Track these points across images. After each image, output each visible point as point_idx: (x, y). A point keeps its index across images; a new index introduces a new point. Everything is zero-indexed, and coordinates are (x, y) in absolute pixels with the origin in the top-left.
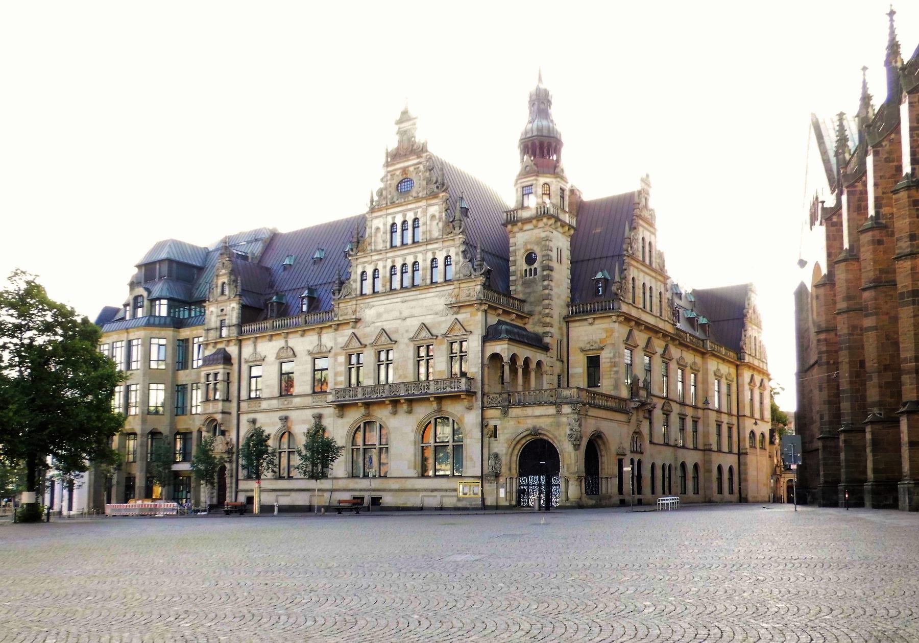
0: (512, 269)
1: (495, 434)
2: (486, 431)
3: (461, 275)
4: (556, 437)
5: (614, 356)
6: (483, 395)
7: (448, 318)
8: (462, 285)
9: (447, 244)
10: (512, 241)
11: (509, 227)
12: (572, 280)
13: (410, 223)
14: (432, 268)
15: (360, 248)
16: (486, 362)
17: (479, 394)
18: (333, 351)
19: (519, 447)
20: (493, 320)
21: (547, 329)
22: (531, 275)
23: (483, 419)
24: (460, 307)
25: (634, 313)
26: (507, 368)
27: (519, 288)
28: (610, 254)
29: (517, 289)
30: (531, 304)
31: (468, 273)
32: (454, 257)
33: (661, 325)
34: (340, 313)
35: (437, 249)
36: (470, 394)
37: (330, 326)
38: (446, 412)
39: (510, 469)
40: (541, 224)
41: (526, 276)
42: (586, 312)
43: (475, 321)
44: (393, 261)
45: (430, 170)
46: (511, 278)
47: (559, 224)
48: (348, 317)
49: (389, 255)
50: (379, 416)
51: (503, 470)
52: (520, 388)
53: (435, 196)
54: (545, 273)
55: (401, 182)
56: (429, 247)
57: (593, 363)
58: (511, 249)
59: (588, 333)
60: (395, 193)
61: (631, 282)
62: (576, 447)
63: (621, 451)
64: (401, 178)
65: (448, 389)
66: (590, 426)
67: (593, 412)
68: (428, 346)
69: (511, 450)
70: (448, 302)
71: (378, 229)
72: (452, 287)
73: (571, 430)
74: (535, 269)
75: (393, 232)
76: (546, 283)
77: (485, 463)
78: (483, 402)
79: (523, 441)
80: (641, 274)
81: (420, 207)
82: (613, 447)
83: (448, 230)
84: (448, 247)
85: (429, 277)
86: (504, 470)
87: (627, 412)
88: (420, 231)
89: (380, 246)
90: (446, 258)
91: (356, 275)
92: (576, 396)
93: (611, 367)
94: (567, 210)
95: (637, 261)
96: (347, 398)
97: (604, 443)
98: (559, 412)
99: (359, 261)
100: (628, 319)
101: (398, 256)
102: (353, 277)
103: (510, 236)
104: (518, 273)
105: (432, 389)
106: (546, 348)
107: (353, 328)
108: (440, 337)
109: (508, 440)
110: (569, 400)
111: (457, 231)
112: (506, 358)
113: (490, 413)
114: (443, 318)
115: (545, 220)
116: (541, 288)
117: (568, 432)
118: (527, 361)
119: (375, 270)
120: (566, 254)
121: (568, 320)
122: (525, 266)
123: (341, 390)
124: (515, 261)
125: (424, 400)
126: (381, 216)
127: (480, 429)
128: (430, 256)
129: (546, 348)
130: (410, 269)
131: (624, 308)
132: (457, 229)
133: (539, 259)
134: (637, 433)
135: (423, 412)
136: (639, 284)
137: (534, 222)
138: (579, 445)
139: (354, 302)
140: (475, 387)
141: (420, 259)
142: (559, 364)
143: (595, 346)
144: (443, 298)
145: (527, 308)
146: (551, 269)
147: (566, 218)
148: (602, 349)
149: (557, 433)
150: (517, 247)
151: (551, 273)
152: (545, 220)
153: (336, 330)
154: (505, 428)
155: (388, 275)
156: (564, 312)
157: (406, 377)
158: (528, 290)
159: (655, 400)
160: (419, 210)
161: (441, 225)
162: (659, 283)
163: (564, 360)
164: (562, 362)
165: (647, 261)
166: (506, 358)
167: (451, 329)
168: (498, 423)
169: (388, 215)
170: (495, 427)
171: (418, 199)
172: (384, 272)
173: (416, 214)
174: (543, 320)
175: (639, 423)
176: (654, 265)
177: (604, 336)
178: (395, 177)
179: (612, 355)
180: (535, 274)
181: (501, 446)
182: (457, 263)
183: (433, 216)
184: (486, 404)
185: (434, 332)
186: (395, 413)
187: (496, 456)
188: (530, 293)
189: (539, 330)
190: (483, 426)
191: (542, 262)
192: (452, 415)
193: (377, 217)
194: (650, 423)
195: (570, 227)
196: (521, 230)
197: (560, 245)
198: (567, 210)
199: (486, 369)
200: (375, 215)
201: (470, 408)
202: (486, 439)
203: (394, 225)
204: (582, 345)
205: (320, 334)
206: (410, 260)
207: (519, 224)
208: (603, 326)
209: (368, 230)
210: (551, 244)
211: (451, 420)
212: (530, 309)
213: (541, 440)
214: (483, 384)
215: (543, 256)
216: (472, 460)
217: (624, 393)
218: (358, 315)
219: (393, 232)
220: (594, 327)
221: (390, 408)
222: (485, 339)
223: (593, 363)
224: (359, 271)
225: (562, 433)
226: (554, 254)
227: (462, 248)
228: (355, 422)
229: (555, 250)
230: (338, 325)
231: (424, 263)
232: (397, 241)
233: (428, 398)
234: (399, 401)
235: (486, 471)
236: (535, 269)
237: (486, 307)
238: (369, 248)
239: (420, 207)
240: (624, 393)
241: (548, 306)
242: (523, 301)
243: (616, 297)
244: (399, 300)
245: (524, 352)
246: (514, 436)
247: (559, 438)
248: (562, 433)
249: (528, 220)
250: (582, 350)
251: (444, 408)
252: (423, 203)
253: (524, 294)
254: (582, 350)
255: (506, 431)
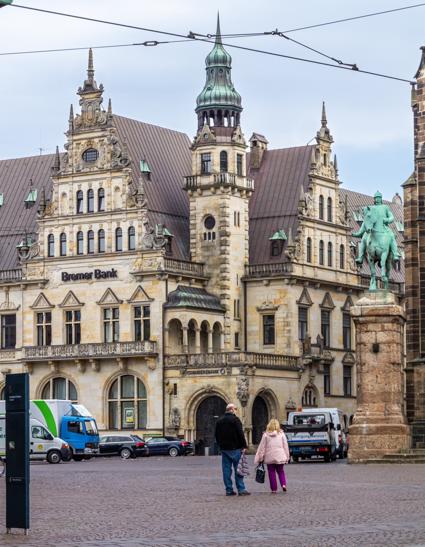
0: (192, 232)
1: (175, 391)
2: (167, 388)
3: (144, 246)
4: (226, 395)
5: (287, 317)
6: (165, 356)
7: (132, 284)
8: (144, 256)
9: (129, 216)
10: (192, 204)
11: (189, 192)
12: (251, 241)
13: (96, 192)
14: (117, 237)
15: (47, 212)
16: (167, 326)
17: (161, 357)
18: (21, 309)
19: (196, 403)
20: (173, 287)
21: (224, 292)
22: (209, 238)
23: (164, 378)
24: (143, 276)
25: (309, 273)
26: (185, 333)
27: (199, 251)
28: (288, 213)
29: (198, 253)
30: (210, 266)
31: (150, 245)
32: (137, 230)
33: (342, 279)
34: (28, 273)
35: (121, 219)
36: (154, 356)
37: (19, 286)
38: (131, 371)
39: (188, 423)
40: (219, 192)
41: (205, 239)
42: (264, 275)
43: (158, 292)
44: (80, 228)
45: (114, 144)
46: (192, 241)
47: (236, 190)
48: (35, 278)
49: (75, 221)
50: (68, 373)
51: (182, 424)
52: (198, 351)
53: (120, 170)
54: (222, 238)
55: (86, 152)
56: (114, 217)
57: (269, 320)
58: (192, 213)
59: (262, 295)
60: (81, 162)
61: (305, 243)
62: (244, 404)
63: (290, 405)
64: (86, 148)
65: (133, 351)
66: (257, 385)
67: (259, 372)
68: (114, 310)
69: (188, 405)
70: (133, 271)
71: (64, 194)
72: (136, 256)
73: (239, 389)
74: (214, 233)
75: (79, 200)
76: (223, 248)
77: (167, 417)
78: (164, 363)
79: (200, 398)
80: (318, 232)
81: (105, 178)
82: (282, 403)
83: (132, 203)
84: (131, 218)
85: (114, 245)
86: (183, 423)
87: (297, 370)
88: (105, 201)
89: (67, 212)
90: (130, 228)
91: (43, 237)
92: (243, 359)
93: (284, 326)
94: (245, 174)
95: (314, 221)
96: (37, 355)
97: (273, 399)
98: (230, 374)
99: (46, 224)
100: (301, 281)
101: (84, 223)
102: (40, 239)
103: (191, 200)
104: (198, 236)
105: (119, 350)
106: (223, 311)
107: (42, 288)
108: (125, 302)
109: (186, 397)
110: (237, 363)
111: (140, 205)
112: (185, 324)
113: (170, 373)
114: (128, 285)
115: (222, 188)
116: (219, 252)
117: (237, 391)
118: (205, 324)
119: (62, 235)
120: (244, 217)
121: (245, 282)
122: (205, 230)
123: (31, 348)
124: (195, 224)
125: (111, 360)
126: (67, 183)
127: (162, 387)
128: (114, 226)
129: (223, 311)
130: (96, 236)
131: (298, 271)
132: (140, 203)
133: (217, 224)
134: (310, 390)
135: (109, 372)
136: (316, 244)
137: (212, 189)
138: (246, 402)
139: (42, 264)
140: (157, 349)
141: (105, 227)
142: (236, 323)
143: (271, 306)
144: (128, 267)
145: (206, 270)
146: (227, 235)
147: (242, 183)
148: (276, 309)
149: (227, 392)
150: (197, 211)
151: (227, 238)
152: (222, 188)
153: (24, 289)
154: (182, 386)
155: (75, 240)
156: (242, 273)
157: (93, 338)
158: (206, 254)
159: (334, 354)
160: (104, 181)
161: (125, 197)
162: (340, 237)
163: (242, 319)
164: (240, 320)
165: (326, 219)
166: (185, 324)
167: (135, 295)
168: (177, 381)
169: (74, 182)
170: (175, 385)
171: (102, 171)
172: (71, 238)
173: (101, 184)
174: (220, 283)
175: (312, 378)
176: (335, 220)
177: (278, 297)
178: (80, 146)
179: (285, 315)
180: (214, 238)
181: (180, 402)
182: (139, 235)
183: (117, 188)
184: (167, 365)
185: (120, 297)
186: (84, 371)
187: (176, 411)
188: (209, 256)
189: (217, 291)
190: (165, 384)
191: (220, 228)
192: (137, 373)
193: (63, 183)
194: (325, 377)
195: (248, 191)
196: (201, 195)
197: (238, 209)
198: (245, 174)
199: (167, 333)
200: (61, 181)
201: (152, 369)
202: (167, 396)
203: (79, 192)
204: (259, 305)
205: (7, 293)
206: (96, 228)
207: (199, 190)
208: (278, 287)
209: (54, 196)
210: (228, 211)
211: (135, 379)
212: (209, 271)
213: (215, 397)
214: (164, 347)
215: (221, 222)
216: (154, 414)
217: (296, 351)
218: (45, 277)
219: (79, 200)
220: (270, 288)
221: (79, 366)
222: (165, 308)
223: (269, 320)
224: (46, 234)
225: (232, 392)
226: (230, 220)
227: (146, 220)
228: (44, 378)
229: (232, 217)
230: (26, 285)
231: (109, 229)
232: (84, 208)
233: (115, 359)
234: (88, 360)
235: (167, 425)
236: (214, 233)
237: (167, 277)
238: (56, 212)
239: (105, 178)
240: (296, 351)
241: (224, 270)
242: (202, 264)
243: (289, 261)
244: (86, 264)
245: (200, 317)
246: (191, 393)
247: (229, 396)
248: (232, 392)
249: (207, 188)
250: (259, 310)
251: (130, 368)
252: (108, 175)
253: (204, 257)
254: (259, 310)
255: (184, 389)
